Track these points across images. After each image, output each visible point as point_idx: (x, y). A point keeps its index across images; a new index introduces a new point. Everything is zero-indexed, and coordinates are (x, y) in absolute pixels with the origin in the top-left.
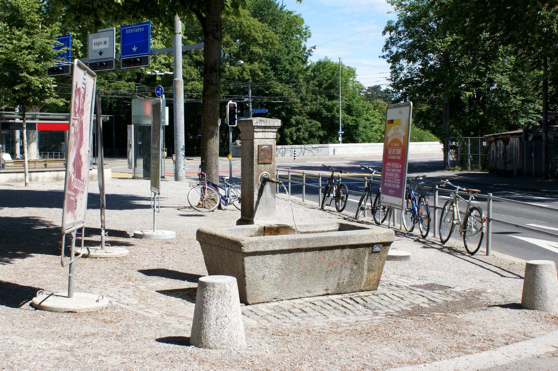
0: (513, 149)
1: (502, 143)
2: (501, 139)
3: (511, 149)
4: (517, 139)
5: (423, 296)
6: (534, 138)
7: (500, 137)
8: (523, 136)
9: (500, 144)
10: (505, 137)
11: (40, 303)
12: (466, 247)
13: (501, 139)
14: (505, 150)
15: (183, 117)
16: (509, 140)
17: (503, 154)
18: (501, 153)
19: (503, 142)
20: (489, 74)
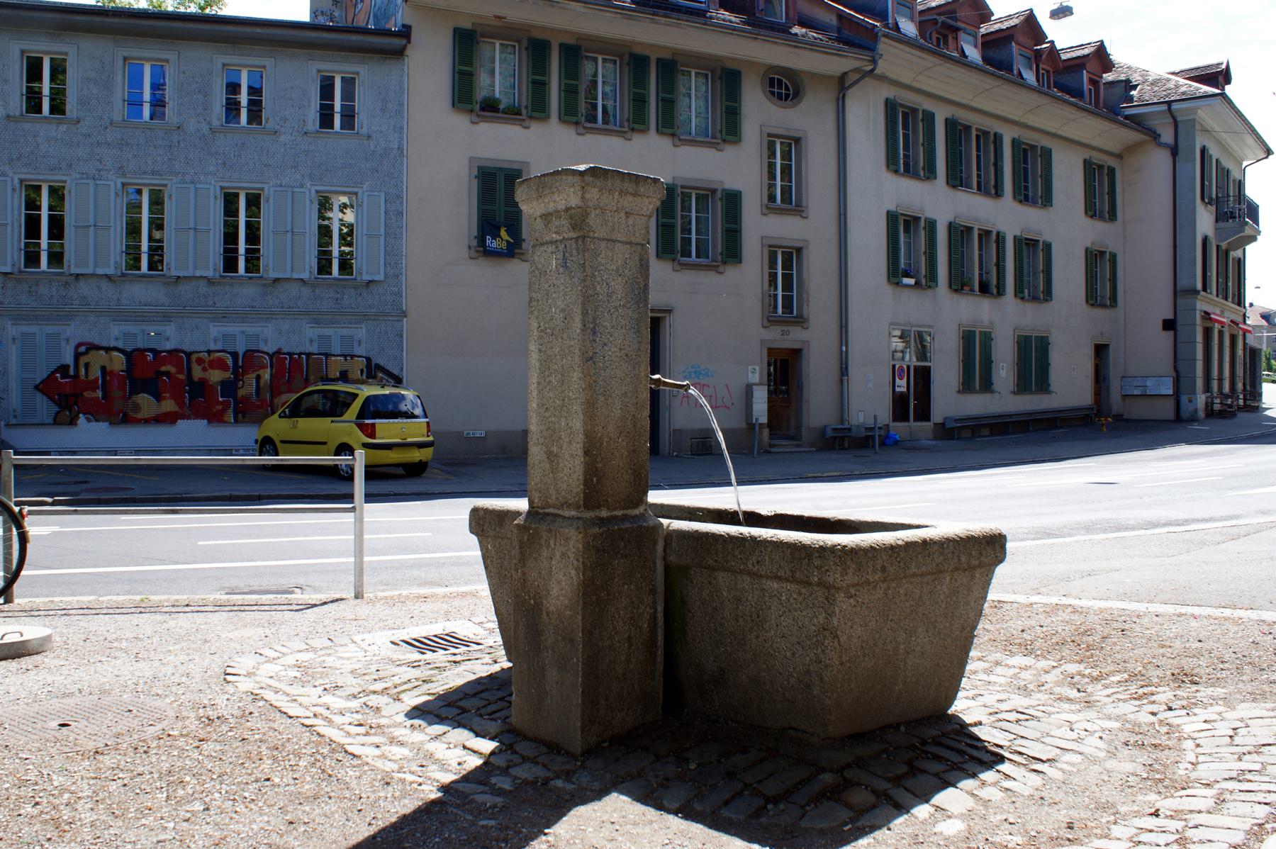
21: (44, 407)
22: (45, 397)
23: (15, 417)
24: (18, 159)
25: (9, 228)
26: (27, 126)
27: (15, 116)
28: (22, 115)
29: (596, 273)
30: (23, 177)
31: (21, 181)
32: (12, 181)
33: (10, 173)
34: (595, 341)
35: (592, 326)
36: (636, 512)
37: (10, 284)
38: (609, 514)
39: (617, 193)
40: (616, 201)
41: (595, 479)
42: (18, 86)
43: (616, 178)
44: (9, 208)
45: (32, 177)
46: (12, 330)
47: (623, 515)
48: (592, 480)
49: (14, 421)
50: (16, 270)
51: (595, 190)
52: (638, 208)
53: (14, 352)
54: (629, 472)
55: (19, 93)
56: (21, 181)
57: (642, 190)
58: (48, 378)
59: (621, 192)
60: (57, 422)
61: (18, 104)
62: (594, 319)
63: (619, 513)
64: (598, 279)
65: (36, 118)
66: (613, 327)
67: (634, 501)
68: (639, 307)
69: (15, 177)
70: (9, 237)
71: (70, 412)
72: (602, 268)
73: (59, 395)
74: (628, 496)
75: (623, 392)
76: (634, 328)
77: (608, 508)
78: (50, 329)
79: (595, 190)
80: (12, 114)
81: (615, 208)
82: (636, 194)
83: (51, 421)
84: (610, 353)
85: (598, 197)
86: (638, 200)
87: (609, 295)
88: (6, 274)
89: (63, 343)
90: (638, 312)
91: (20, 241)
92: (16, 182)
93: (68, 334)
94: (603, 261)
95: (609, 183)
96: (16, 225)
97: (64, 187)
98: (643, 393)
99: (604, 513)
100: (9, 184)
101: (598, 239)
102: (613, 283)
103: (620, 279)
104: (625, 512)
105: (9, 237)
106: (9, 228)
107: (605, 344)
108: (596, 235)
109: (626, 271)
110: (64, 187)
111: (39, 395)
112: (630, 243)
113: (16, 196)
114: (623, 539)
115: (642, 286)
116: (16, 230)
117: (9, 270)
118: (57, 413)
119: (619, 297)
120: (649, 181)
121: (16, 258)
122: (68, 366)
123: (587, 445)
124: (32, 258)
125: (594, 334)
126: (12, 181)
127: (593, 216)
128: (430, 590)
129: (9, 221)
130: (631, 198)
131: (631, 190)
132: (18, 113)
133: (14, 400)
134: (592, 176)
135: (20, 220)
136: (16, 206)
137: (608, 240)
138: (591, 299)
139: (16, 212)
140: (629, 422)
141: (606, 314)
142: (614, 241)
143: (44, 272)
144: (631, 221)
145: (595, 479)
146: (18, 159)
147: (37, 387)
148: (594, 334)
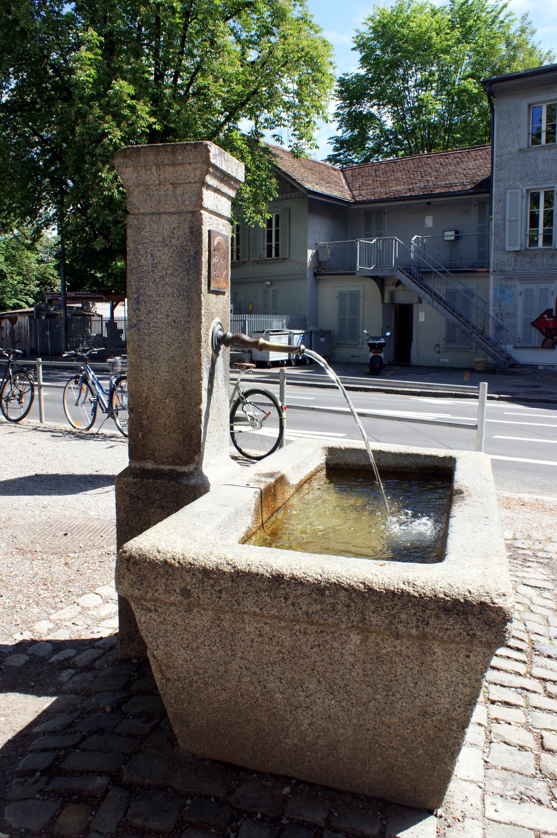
0: (21, 328)
1: (8, 322)
2: (7, 318)
3: (20, 328)
4: (27, 318)
5: (508, 657)
6: (47, 317)
7: (7, 316)
8: (35, 314)
9: (6, 323)
10: (13, 315)
11: (207, 210)
12: (240, 450)
13: (7, 318)
14: (12, 329)
15: (428, 453)
16: (17, 319)
17: (10, 333)
18: (8, 332)
19: (10, 320)
20: (419, 85)
21: (537, 336)
22: (537, 330)
23: (519, 342)
24: (526, 176)
25: (519, 222)
26: (531, 154)
27: (524, 149)
28: (529, 147)
29: (140, 247)
30: (528, 188)
31: (528, 191)
32: (522, 191)
33: (521, 187)
34: (139, 309)
35: (135, 296)
36: (185, 469)
37: (519, 258)
38: (155, 466)
39: (154, 167)
40: (156, 175)
41: (140, 434)
42: (526, 128)
43: (149, 153)
44: (520, 209)
45: (533, 187)
46: (520, 287)
47: (170, 470)
48: (138, 435)
49: (518, 345)
50: (523, 249)
51: (130, 170)
52: (183, 177)
53: (520, 302)
54: (178, 431)
55: (526, 132)
56: (528, 191)
57: (180, 158)
58: (539, 318)
59: (158, 166)
60: (544, 346)
61: (526, 141)
62: (138, 290)
63: (166, 467)
64: (142, 252)
65: (537, 148)
66: (158, 295)
67: (184, 459)
68: (189, 274)
69: (523, 188)
70: (519, 227)
71: (552, 340)
72: (146, 241)
73: (546, 329)
74: (176, 454)
75: (170, 356)
76: (183, 295)
77: (155, 462)
78: (542, 286)
79: (130, 170)
80: (522, 148)
81: (157, 182)
82: (173, 164)
83: (540, 345)
84: (156, 320)
85: (136, 175)
86: (179, 169)
87: (154, 266)
88: (517, 252)
89: (550, 295)
90: (188, 280)
91: (526, 229)
92: (524, 191)
93: (553, 289)
94: (147, 235)
95: (142, 160)
96: (523, 219)
97: (553, 191)
98: (193, 358)
99: (150, 465)
100: (520, 193)
101: (143, 214)
102: (158, 254)
103: (166, 249)
104: (173, 467)
105: (519, 227)
106: (519, 222)
107: (150, 312)
108: (142, 211)
109: (174, 241)
110: (553, 191)
111: (534, 329)
112: (180, 213)
113: (524, 200)
114: (158, 491)
115: (192, 253)
116: (524, 223)
117: (518, 248)
118: (544, 341)
119: (166, 266)
120: (188, 147)
121: (523, 241)
122: (552, 310)
123: (132, 403)
124: (533, 242)
125: (138, 303)
126: (522, 191)
127: (136, 194)
128: (535, 497)
129: (519, 218)
130: (171, 169)
131: (167, 161)
132: (526, 146)
133: (520, 331)
134: (122, 158)
135: (527, 216)
136: (524, 207)
137: (153, 214)
138: (134, 271)
139: (524, 212)
140: (177, 385)
141: (151, 284)
142: (159, 214)
143: (540, 249)
144: (179, 191)
145: (140, 434)
146: (526, 176)
147: (533, 324)
148: (138, 303)
